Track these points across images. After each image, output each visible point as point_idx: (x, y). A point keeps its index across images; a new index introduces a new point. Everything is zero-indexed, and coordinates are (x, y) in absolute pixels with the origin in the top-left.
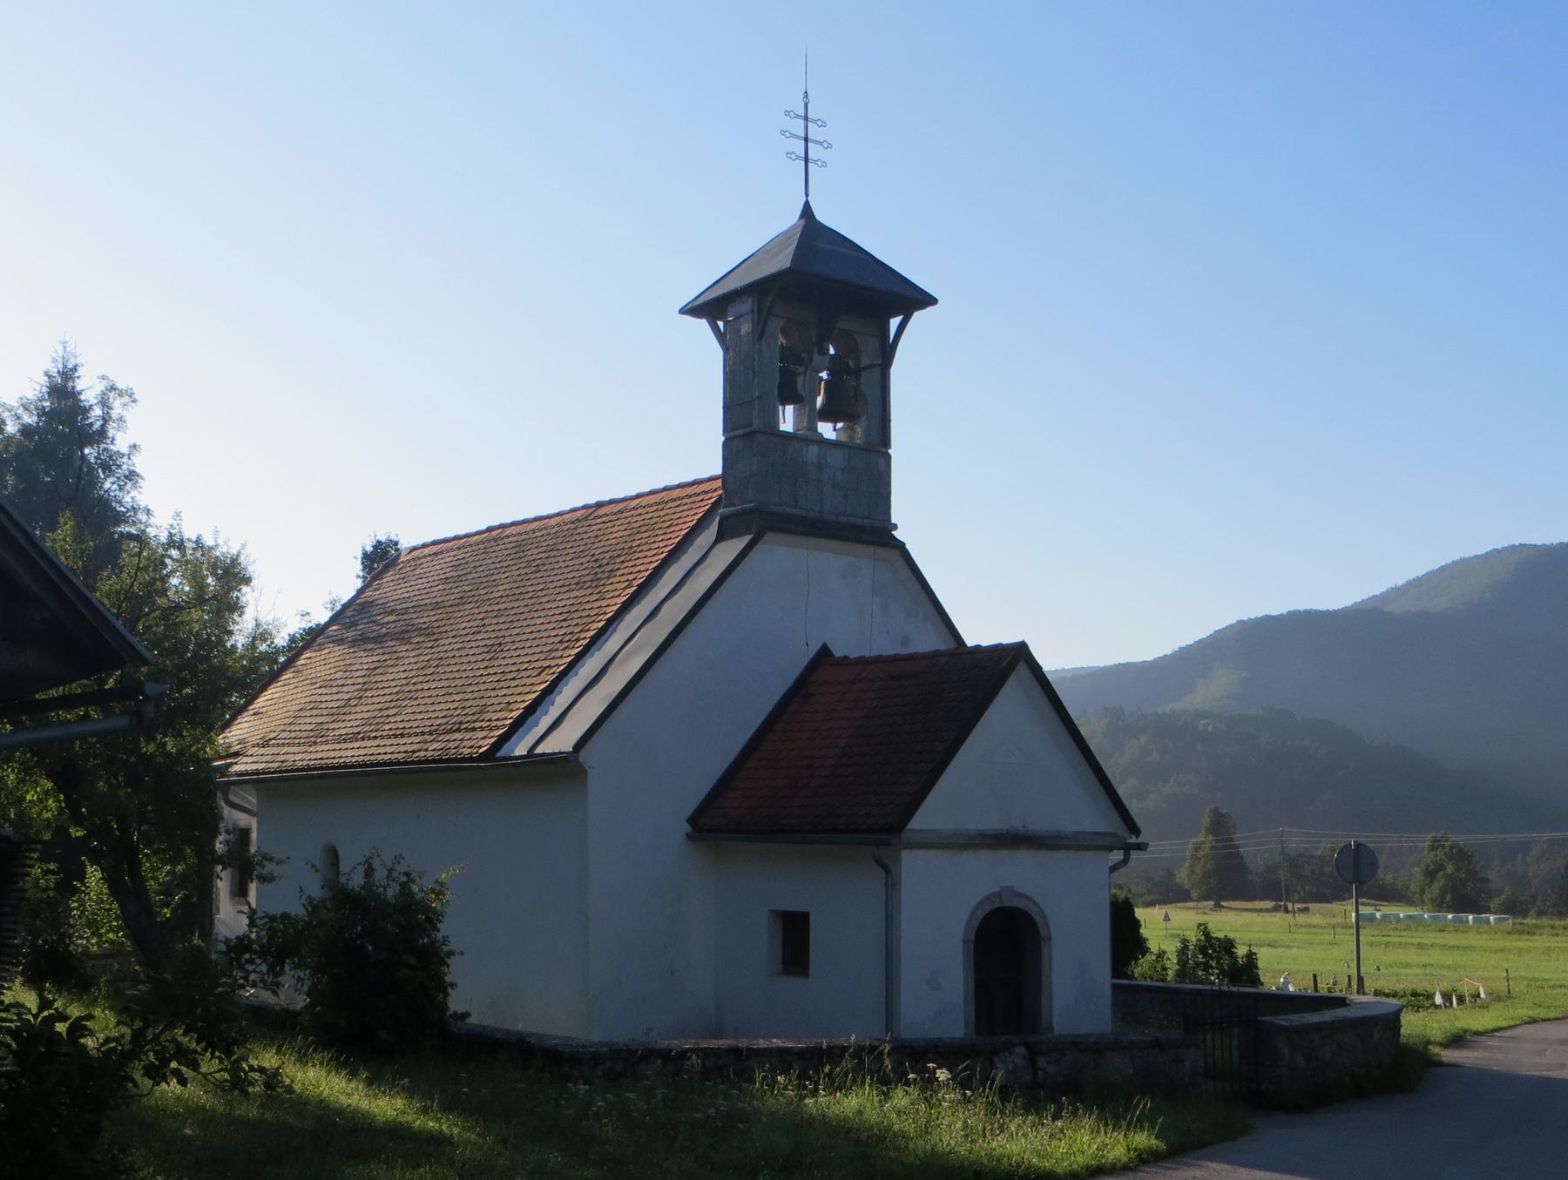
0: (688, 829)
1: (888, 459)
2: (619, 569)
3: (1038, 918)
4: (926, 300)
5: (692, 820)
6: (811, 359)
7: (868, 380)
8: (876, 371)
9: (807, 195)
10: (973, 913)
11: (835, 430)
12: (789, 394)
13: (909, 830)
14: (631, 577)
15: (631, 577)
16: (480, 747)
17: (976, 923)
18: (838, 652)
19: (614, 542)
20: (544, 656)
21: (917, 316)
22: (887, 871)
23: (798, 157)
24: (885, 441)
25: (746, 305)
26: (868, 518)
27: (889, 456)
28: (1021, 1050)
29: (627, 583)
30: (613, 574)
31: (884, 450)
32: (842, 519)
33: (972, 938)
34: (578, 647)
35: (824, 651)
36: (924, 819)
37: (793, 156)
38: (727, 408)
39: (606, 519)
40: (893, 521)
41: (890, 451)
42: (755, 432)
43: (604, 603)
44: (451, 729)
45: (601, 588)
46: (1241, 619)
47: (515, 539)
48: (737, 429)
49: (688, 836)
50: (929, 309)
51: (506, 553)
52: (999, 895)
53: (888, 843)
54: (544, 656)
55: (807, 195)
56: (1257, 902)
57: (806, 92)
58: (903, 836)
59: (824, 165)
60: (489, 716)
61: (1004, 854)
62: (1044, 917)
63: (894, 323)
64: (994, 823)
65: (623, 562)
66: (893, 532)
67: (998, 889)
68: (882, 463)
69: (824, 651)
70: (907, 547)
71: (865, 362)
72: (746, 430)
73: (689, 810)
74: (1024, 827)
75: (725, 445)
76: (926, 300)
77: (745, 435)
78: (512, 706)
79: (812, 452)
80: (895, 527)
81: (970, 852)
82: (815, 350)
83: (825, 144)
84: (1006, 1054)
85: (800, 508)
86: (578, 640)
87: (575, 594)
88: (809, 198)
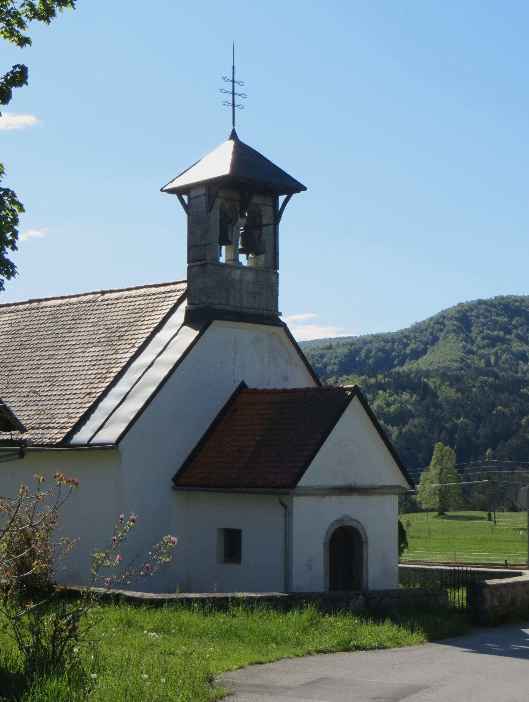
0: (173, 484)
1: (277, 275)
2: (124, 335)
3: (361, 532)
4: (299, 188)
5: (176, 479)
6: (236, 221)
7: (267, 231)
8: (271, 228)
9: (234, 126)
10: (329, 529)
11: (248, 259)
12: (225, 240)
13: (300, 487)
14: (134, 341)
15: (134, 341)
16: (56, 439)
17: (330, 535)
18: (251, 385)
19: (119, 317)
20: (86, 386)
21: (295, 196)
22: (286, 507)
23: (229, 104)
24: (275, 265)
25: (202, 191)
26: (266, 310)
27: (278, 274)
28: (361, 597)
29: (131, 345)
30: (121, 338)
31: (275, 271)
32: (253, 311)
33: (328, 542)
34: (106, 383)
35: (243, 385)
36: (303, 482)
37: (227, 104)
38: (190, 248)
39: (109, 302)
40: (279, 311)
41: (278, 271)
42: (207, 264)
43: (119, 356)
44: (35, 426)
45: (115, 347)
46: (460, 302)
47: (49, 309)
48: (197, 261)
49: (173, 488)
50: (302, 193)
51: (46, 318)
52: (341, 520)
53: (288, 494)
54: (86, 386)
55: (234, 126)
56: (469, 512)
57: (233, 66)
58: (295, 490)
59: (243, 107)
60: (58, 420)
61: (345, 498)
62: (363, 529)
63: (282, 199)
64: (339, 482)
65: (126, 331)
66: (279, 317)
67: (341, 517)
68: (274, 278)
69: (243, 385)
70: (288, 326)
71: (265, 221)
72: (202, 262)
73: (173, 473)
74: (355, 483)
75: (189, 269)
76: (299, 188)
77: (201, 265)
78: (71, 415)
79: (237, 274)
80: (281, 314)
81: (328, 497)
82: (239, 215)
83: (244, 96)
84: (355, 599)
85: (231, 306)
86: (106, 378)
87: (98, 349)
88: (235, 127)
